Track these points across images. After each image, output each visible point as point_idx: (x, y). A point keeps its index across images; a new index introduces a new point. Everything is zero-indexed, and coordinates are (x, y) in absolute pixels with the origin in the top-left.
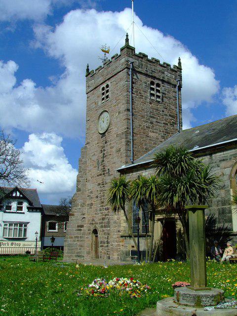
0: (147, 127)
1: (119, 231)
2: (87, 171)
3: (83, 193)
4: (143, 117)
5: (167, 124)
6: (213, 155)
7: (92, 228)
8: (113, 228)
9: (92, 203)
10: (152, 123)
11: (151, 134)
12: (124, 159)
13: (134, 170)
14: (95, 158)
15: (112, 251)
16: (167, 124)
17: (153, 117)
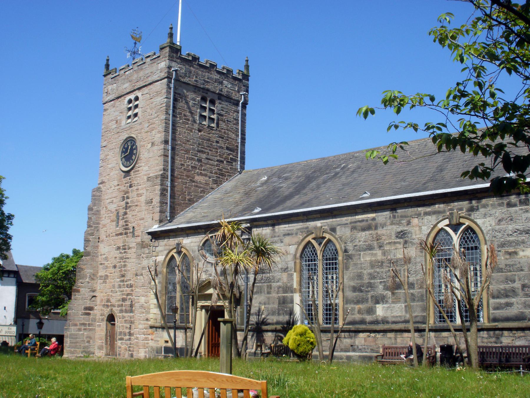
0: (192, 167)
1: (147, 320)
2: (101, 226)
3: (93, 260)
4: (187, 151)
5: (222, 162)
6: (276, 227)
7: (107, 312)
8: (138, 315)
9: (107, 276)
10: (200, 161)
11: (198, 178)
12: (157, 216)
13: (171, 234)
14: (113, 207)
15: (138, 346)
16: (222, 162)
17: (202, 152)
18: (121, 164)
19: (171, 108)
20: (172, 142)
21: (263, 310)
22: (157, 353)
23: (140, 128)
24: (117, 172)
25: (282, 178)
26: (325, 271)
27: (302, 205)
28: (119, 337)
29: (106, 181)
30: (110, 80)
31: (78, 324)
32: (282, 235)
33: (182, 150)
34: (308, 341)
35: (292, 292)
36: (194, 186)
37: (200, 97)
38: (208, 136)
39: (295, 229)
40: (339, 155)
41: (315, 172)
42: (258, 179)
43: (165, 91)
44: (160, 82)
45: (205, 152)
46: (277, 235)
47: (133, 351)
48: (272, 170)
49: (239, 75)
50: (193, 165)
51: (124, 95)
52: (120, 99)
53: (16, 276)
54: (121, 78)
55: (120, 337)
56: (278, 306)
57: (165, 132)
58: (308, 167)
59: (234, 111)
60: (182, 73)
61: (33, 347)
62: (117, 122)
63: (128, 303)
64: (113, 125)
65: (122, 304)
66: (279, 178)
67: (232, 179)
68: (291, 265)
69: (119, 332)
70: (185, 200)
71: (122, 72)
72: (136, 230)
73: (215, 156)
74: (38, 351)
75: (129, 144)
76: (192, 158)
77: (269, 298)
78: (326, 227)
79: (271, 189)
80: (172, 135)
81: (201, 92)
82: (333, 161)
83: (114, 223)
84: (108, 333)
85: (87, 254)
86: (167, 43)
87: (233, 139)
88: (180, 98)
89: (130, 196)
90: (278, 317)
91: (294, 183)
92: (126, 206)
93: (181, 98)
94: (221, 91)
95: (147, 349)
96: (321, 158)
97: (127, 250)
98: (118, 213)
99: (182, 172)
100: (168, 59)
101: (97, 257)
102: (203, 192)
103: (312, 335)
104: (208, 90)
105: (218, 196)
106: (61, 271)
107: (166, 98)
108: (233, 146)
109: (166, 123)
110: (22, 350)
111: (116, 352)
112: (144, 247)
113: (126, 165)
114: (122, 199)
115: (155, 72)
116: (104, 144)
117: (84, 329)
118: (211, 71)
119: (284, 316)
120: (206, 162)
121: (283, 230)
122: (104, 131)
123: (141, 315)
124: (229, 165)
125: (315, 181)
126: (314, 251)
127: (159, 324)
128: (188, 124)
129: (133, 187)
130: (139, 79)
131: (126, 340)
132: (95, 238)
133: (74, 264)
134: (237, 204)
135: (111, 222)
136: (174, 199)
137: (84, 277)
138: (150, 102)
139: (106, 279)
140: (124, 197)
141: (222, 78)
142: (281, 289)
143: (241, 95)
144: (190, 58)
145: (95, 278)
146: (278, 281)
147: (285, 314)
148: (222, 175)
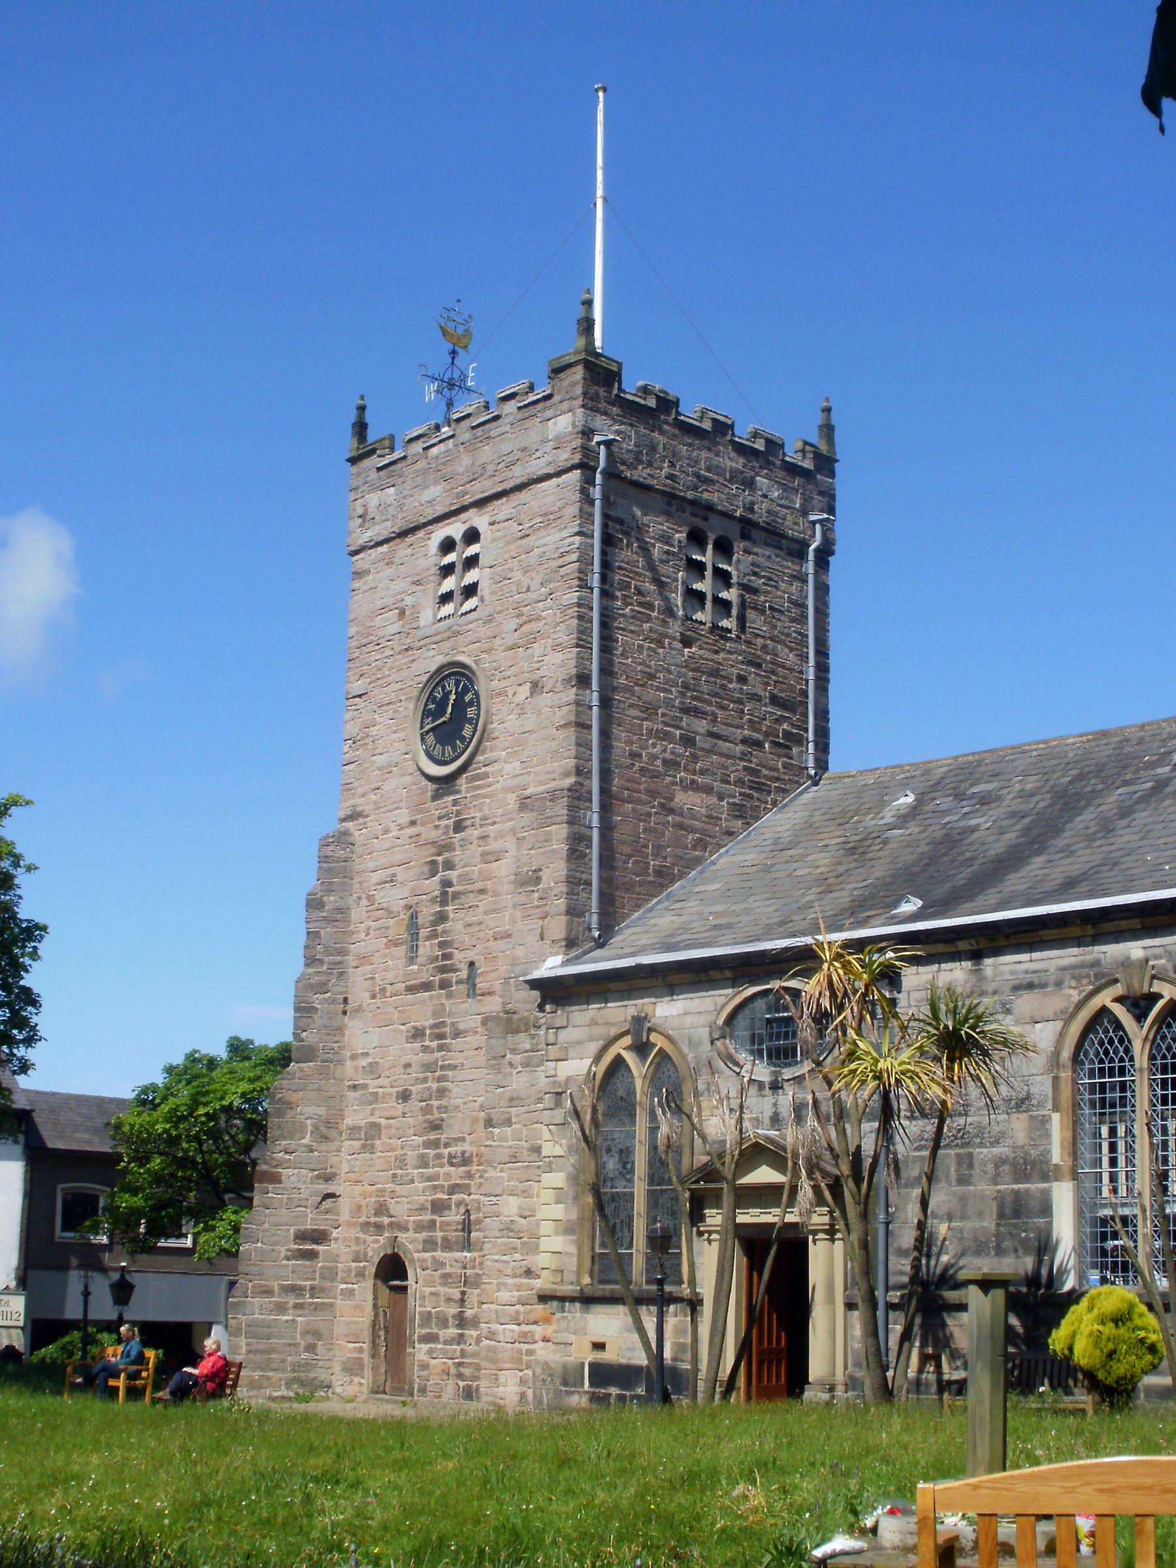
0: (665, 761)
1: (528, 1273)
2: (351, 960)
3: (324, 1073)
4: (649, 710)
5: (758, 744)
7: (376, 1247)
9: (375, 1126)
10: (688, 741)
11: (685, 800)
12: (558, 927)
13: (613, 986)
14: (394, 898)
15: (494, 1361)
18: (422, 753)
19: (597, 567)
20: (600, 679)
21: (945, 1239)
22: (565, 1383)
23: (489, 634)
24: (408, 779)
25: (971, 798)
26: (1160, 1107)
27: (1067, 889)
28: (419, 1331)
29: (367, 809)
30: (374, 475)
31: (276, 1289)
32: (1006, 989)
33: (632, 706)
34: (1142, 1341)
35: (1045, 1177)
36: (674, 826)
37: (685, 529)
38: (712, 660)
39: (1052, 970)
40: (1157, 722)
41: (1081, 777)
42: (882, 804)
43: (573, 510)
44: (555, 481)
45: (705, 713)
46: (991, 987)
47: (475, 1378)
48: (927, 772)
49: (804, 457)
50: (667, 755)
51: (425, 525)
52: (410, 539)
53: (23, 1128)
54: (413, 467)
55: (424, 1331)
56: (998, 1225)
57: (578, 646)
58: (1053, 762)
59: (792, 577)
60: (629, 451)
61: (134, 1368)
62: (402, 613)
63: (454, 1217)
64: (390, 625)
65: (433, 1222)
66: (959, 796)
67: (792, 801)
68: (1042, 1086)
69: (421, 1314)
70: (644, 871)
71: (418, 447)
72: (482, 973)
73: (737, 727)
74: (150, 1381)
75: (450, 685)
76: (666, 733)
77: (963, 1199)
78: (1163, 961)
79: (939, 834)
80: (601, 658)
81: (687, 515)
82: (1141, 741)
83: (401, 951)
84: (381, 1318)
85: (309, 1054)
86: (577, 352)
87: (791, 670)
88: (625, 533)
89: (457, 860)
90: (996, 1260)
91: (1012, 815)
92: (444, 894)
93: (627, 534)
94: (750, 508)
95: (529, 1372)
96: (1097, 733)
97: (448, 1041)
98: (414, 917)
99: (633, 780)
100: (583, 406)
101: (341, 1062)
102: (700, 844)
103: (1151, 1320)
104: (709, 508)
105: (752, 857)
106: (202, 1111)
107: (579, 533)
108: (791, 691)
109: (580, 617)
110: (96, 1376)
111: (411, 1383)
112: (516, 1031)
113: (440, 757)
114: (426, 869)
115: (535, 446)
116: (358, 686)
117: (297, 1306)
118: (717, 444)
119: (1018, 1257)
120: (707, 746)
121: (1012, 973)
122: (355, 643)
123: (505, 1258)
124: (779, 756)
125: (1092, 809)
126: (1121, 1041)
127: (571, 1287)
128: (649, 619)
129: (469, 831)
130: (479, 470)
131: (446, 1342)
132: (334, 1001)
133: (244, 1087)
134: (826, 885)
135: (387, 946)
136: (613, 868)
137: (297, 1131)
138: (520, 547)
139: (373, 1138)
140: (433, 863)
141: (753, 468)
142: (1006, 1168)
143: (814, 523)
144: (652, 402)
145: (333, 1133)
146: (997, 1142)
147: (1020, 1253)
148: (759, 787)
